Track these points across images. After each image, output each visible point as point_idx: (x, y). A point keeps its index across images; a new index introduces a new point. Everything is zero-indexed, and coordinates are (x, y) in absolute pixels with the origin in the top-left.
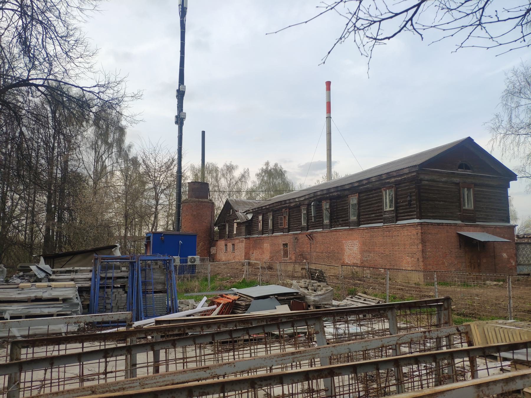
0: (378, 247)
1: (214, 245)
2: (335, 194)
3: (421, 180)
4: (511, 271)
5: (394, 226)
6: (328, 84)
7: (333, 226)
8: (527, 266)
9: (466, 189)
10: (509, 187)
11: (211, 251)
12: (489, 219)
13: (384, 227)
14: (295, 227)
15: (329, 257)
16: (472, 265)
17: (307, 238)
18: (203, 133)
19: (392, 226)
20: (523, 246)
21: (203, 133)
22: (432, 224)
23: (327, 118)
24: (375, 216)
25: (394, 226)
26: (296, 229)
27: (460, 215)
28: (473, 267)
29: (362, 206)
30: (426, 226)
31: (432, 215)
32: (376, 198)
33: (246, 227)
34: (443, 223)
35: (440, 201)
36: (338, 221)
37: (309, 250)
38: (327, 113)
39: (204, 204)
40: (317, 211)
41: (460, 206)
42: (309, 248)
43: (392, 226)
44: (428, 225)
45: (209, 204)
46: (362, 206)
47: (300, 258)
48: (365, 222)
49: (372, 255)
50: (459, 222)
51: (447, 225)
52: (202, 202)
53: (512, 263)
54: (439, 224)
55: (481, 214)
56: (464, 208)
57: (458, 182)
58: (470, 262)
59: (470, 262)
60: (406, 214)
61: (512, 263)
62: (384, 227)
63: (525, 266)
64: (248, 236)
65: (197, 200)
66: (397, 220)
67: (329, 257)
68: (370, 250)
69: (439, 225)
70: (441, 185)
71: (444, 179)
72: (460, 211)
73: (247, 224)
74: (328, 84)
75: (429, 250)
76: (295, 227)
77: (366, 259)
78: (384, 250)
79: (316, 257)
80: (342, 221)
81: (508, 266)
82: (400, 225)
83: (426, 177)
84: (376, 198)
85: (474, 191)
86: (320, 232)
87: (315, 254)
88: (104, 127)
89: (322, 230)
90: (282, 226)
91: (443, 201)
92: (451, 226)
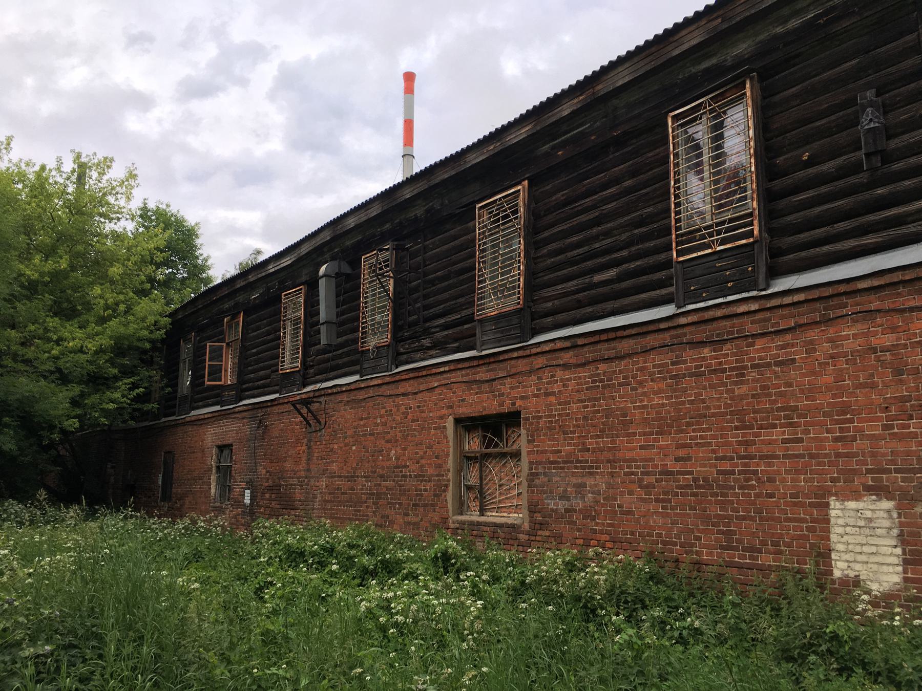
0: (638, 441)
2: (419, 211)
5: (754, 307)
6: (409, 78)
7: (403, 358)
13: (683, 320)
14: (262, 379)
15: (379, 496)
17: (300, 419)
19: (743, 308)
24: (620, 279)
25: (754, 307)
26: (264, 386)
29: (547, 241)
32: (628, 183)
36: (427, 332)
37: (303, 466)
40: (343, 313)
42: (304, 460)
43: (743, 308)
46: (547, 241)
47: (270, 500)
48: (560, 317)
49: (600, 482)
60: (843, 226)
62: (683, 320)
66: (775, 273)
67: (379, 496)
68: (587, 456)
74: (409, 78)
76: (262, 379)
77: (562, 505)
78: (682, 453)
79: (328, 497)
80: (446, 327)
82: (801, 297)
84: (628, 183)
86: (350, 389)
87: (323, 483)
88: (357, 522)
89: (357, 377)
90: (220, 380)
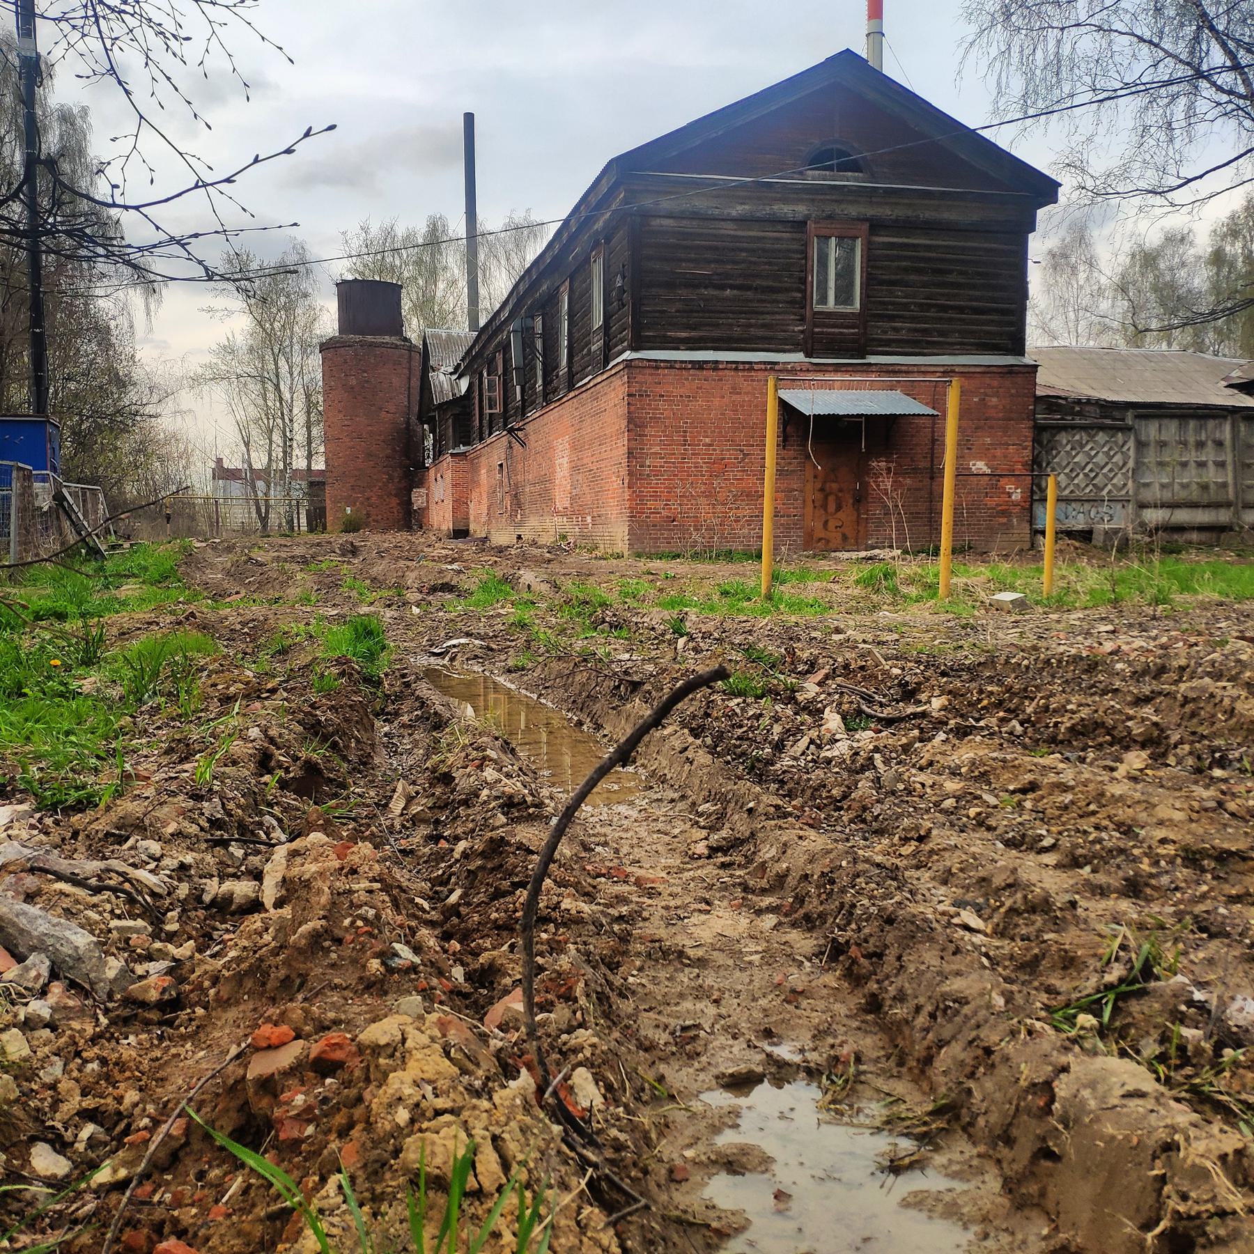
1: (421, 483)
3: (646, 215)
4: (1005, 520)
8: (1087, 506)
9: (833, 241)
10: (1033, 230)
11: (413, 499)
12: (928, 342)
16: (831, 499)
18: (469, 119)
20: (1077, 437)
21: (469, 119)
22: (671, 364)
23: (868, 35)
27: (802, 332)
28: (832, 507)
30: (648, 371)
31: (684, 335)
33: (456, 418)
34: (717, 362)
35: (722, 287)
38: (870, 17)
39: (378, 351)
41: (803, 302)
44: (657, 368)
45: (397, 352)
50: (799, 357)
51: (736, 369)
52: (372, 345)
53: (1010, 495)
54: (699, 365)
55: (896, 330)
56: (818, 308)
57: (799, 217)
58: (822, 490)
59: (822, 490)
61: (1010, 495)
63: (1074, 505)
64: (463, 448)
65: (358, 338)
69: (701, 368)
70: (729, 229)
71: (739, 210)
72: (802, 319)
73: (457, 410)
75: (656, 449)
81: (991, 502)
83: (666, 204)
85: (869, 249)
91: (732, 287)
92: (752, 369)
